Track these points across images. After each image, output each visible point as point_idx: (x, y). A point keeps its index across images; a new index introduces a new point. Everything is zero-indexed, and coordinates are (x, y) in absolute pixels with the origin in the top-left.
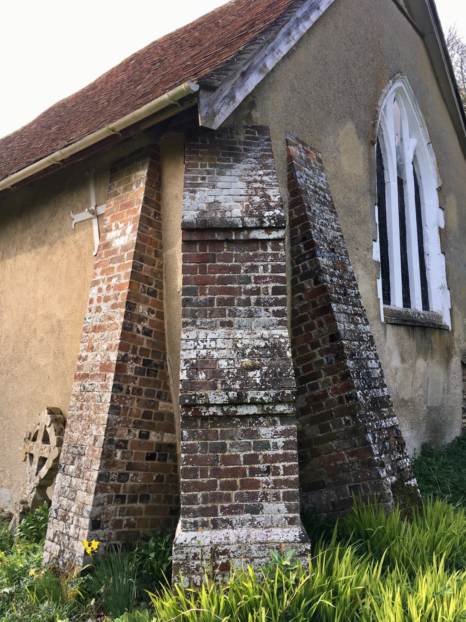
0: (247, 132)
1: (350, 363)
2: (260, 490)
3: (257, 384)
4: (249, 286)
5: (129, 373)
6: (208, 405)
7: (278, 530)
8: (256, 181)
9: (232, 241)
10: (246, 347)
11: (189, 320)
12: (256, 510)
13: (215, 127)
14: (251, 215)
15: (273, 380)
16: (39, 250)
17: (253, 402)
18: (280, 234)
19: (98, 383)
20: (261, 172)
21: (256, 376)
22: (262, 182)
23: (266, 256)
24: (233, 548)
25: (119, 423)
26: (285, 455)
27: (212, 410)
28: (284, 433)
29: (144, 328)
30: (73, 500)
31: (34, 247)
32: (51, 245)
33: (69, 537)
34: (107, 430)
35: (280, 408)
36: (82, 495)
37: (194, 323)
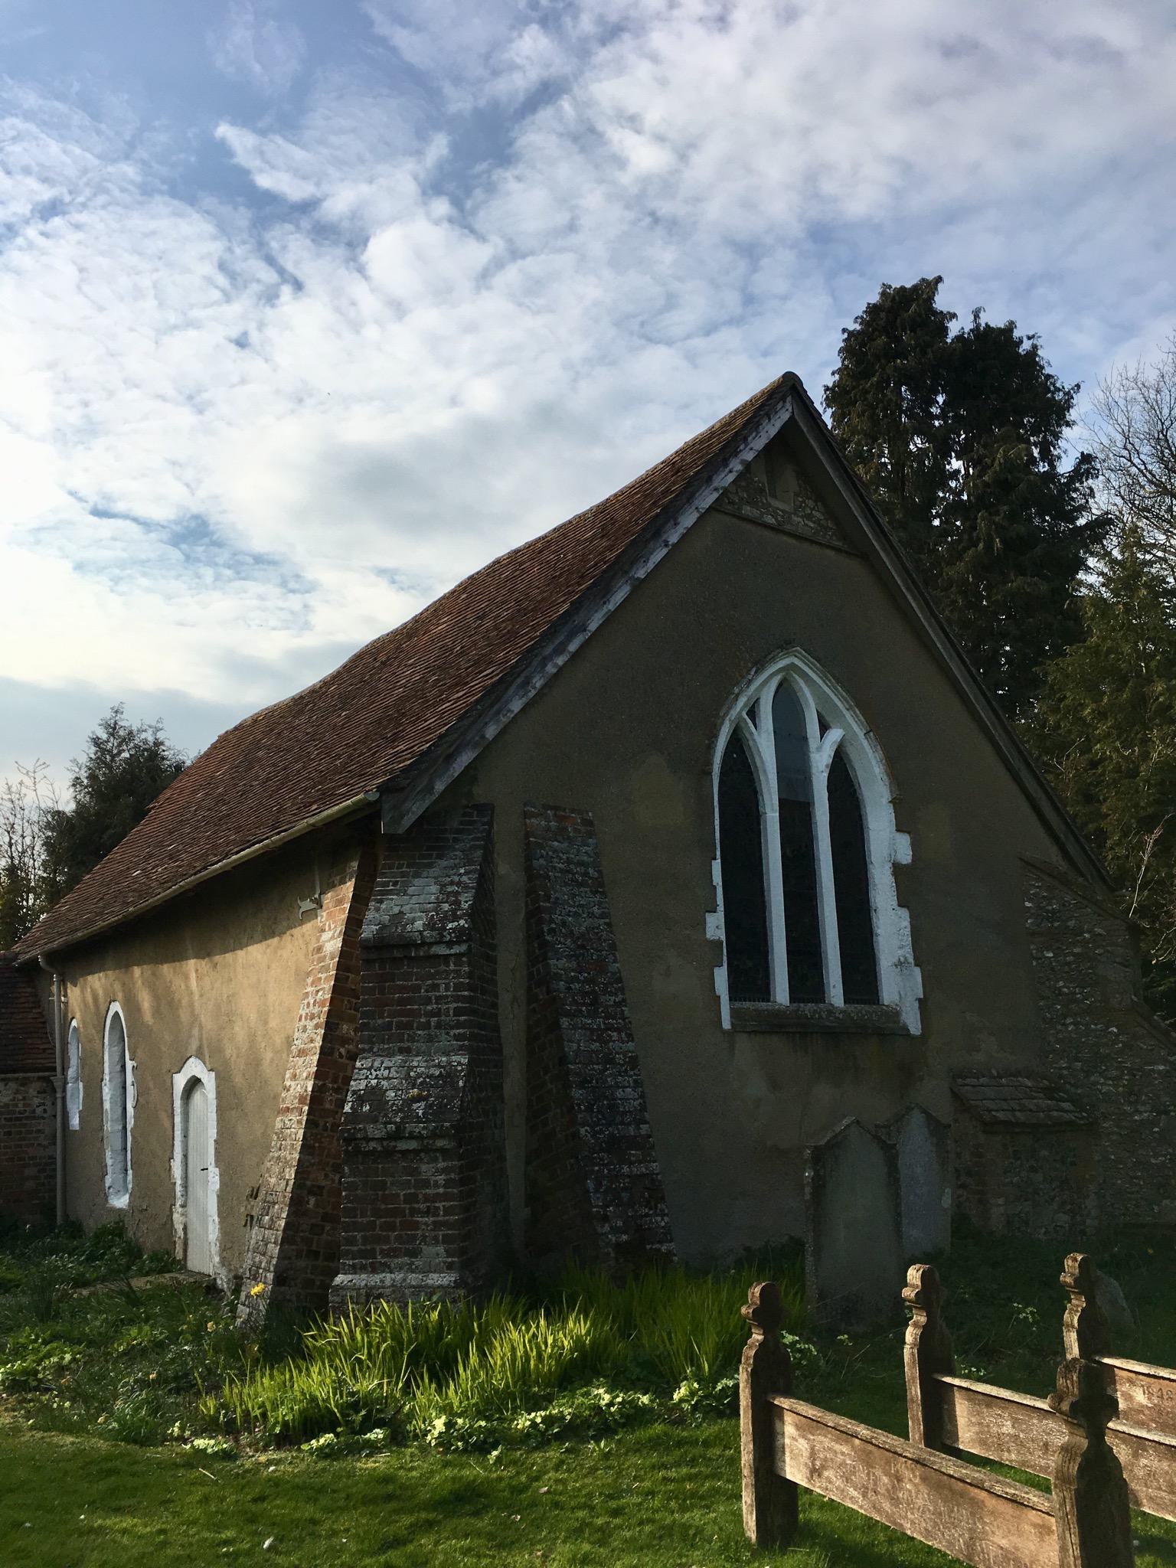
0: (465, 814)
1: (577, 1093)
2: (419, 1232)
3: (418, 1117)
4: (429, 1008)
5: (328, 1106)
7: (435, 1276)
8: (452, 883)
9: (411, 958)
10: (419, 1076)
11: (366, 1047)
12: (414, 1253)
13: (401, 831)
14: (433, 929)
15: (437, 1112)
17: (412, 1137)
18: (463, 948)
19: (295, 1117)
20: (462, 871)
21: (419, 1108)
22: (458, 884)
23: (448, 973)
24: (388, 1291)
25: (313, 1165)
26: (445, 1194)
27: (373, 1144)
28: (444, 1171)
29: (348, 1052)
34: (297, 1173)
35: (440, 1143)
37: (370, 1050)
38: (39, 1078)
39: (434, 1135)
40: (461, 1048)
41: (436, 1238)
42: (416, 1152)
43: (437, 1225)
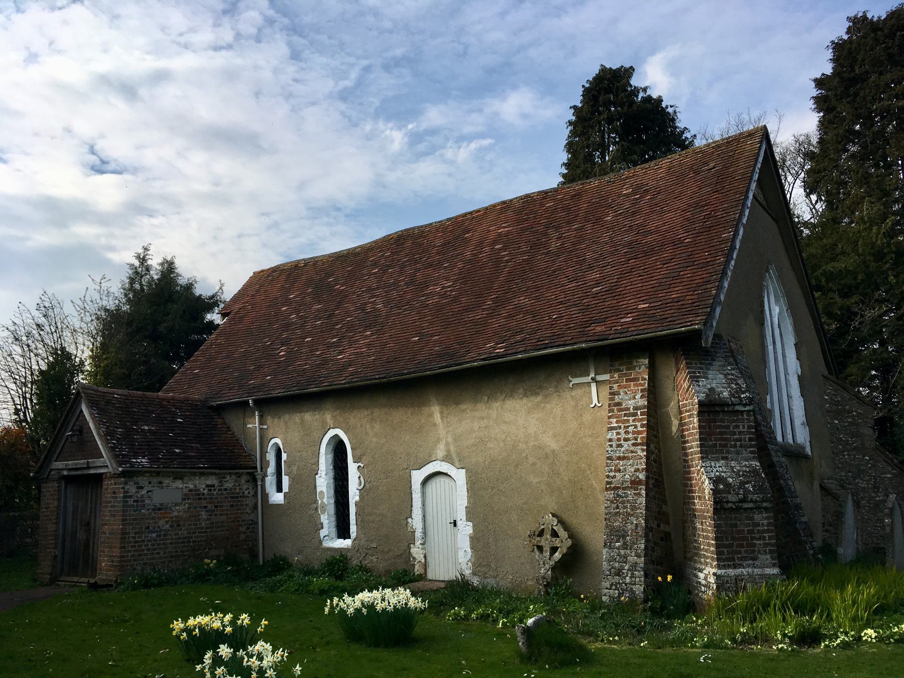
6: (728, 502)
10: (739, 471)
12: (754, 559)
15: (759, 489)
16: (532, 398)
17: (751, 501)
18: (751, 408)
28: (767, 518)
30: (625, 562)
31: (525, 395)
32: (546, 397)
33: (626, 584)
35: (765, 505)
36: (632, 559)
37: (707, 457)
38: (248, 473)
39: (763, 501)
40: (754, 458)
41: (765, 551)
42: (751, 509)
43: (766, 545)
